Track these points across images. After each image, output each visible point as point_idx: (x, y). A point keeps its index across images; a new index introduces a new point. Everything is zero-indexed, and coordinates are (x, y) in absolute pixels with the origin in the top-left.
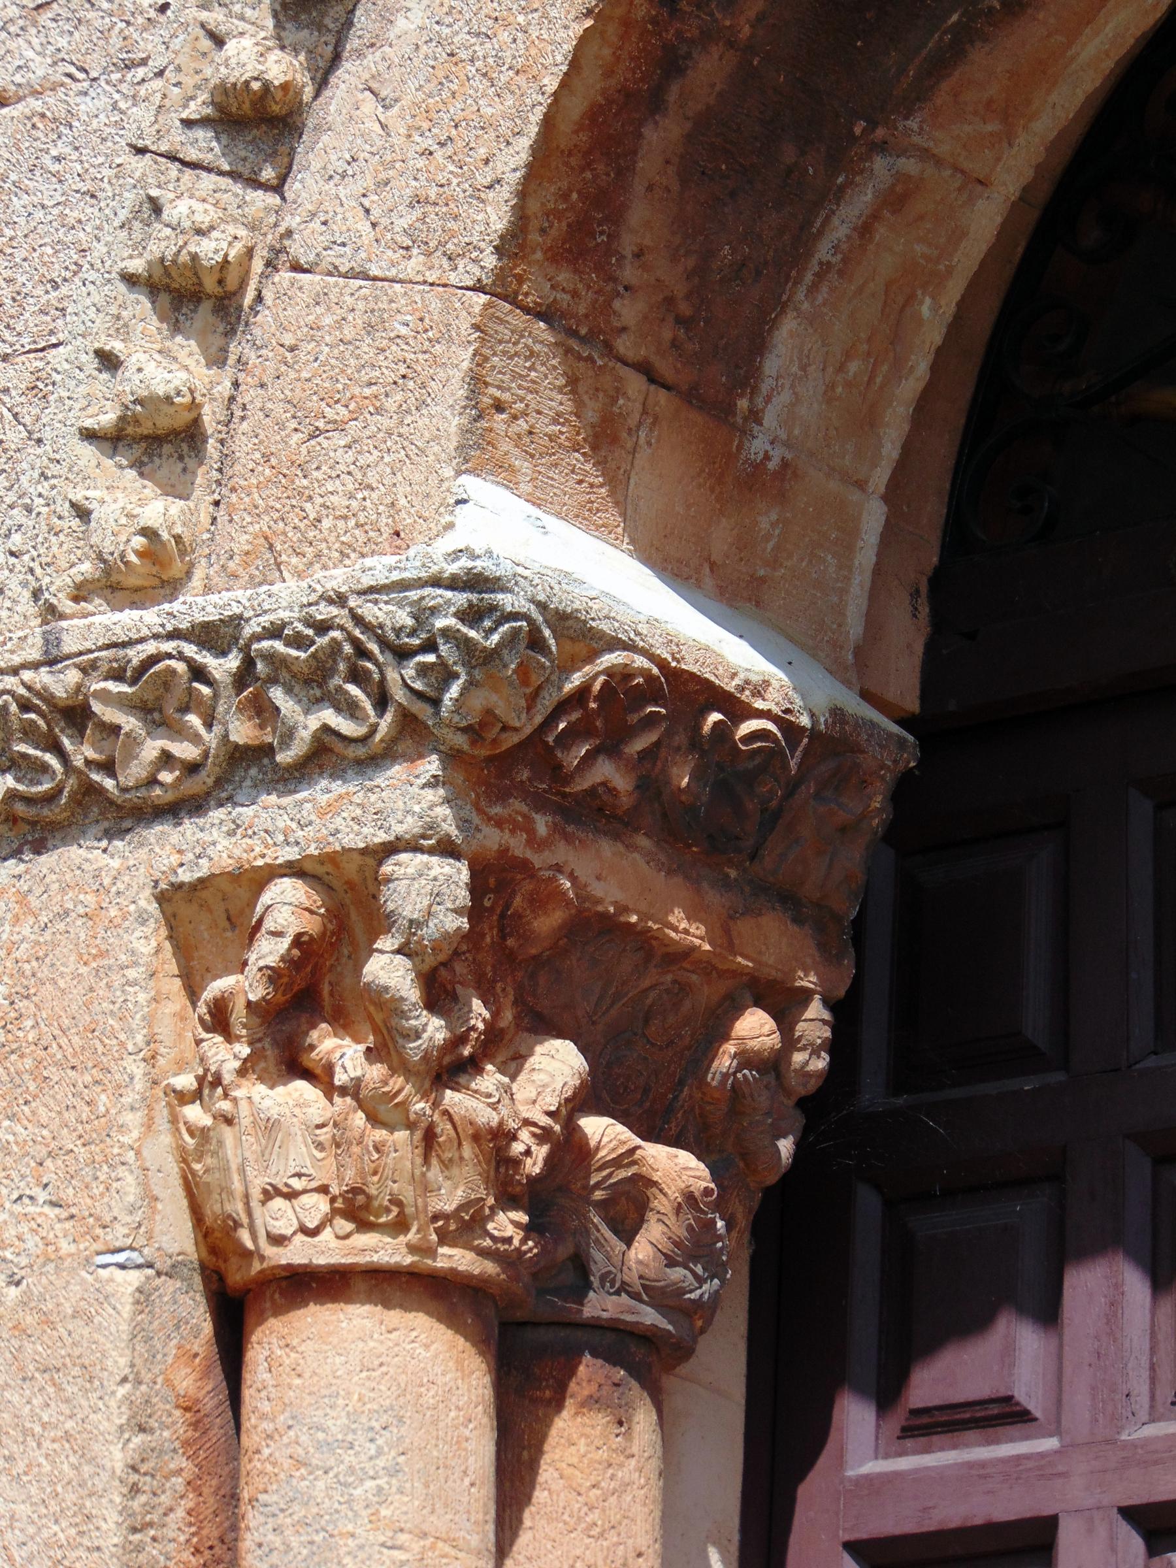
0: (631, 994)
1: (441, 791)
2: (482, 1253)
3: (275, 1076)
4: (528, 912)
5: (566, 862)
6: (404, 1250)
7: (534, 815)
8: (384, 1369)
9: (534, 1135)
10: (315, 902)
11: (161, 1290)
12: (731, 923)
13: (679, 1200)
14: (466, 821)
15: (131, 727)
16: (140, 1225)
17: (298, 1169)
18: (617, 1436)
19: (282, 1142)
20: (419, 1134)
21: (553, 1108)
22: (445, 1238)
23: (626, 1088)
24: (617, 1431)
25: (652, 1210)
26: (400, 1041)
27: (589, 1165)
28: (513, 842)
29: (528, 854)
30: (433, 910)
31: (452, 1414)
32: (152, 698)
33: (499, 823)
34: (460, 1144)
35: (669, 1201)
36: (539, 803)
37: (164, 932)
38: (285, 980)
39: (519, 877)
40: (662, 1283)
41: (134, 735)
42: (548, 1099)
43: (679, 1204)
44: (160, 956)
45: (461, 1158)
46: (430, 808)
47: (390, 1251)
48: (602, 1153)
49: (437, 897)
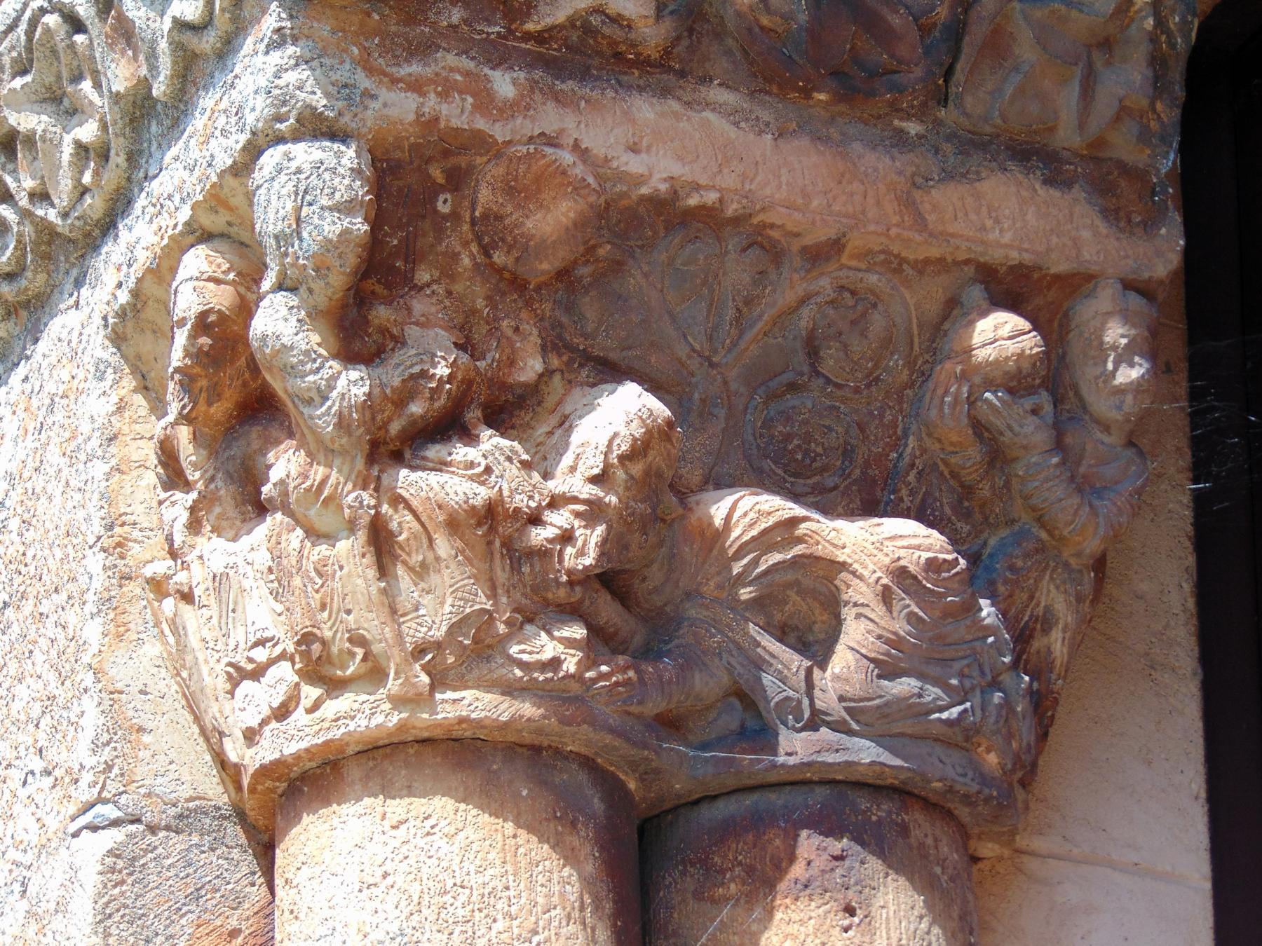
0: (766, 317)
1: (291, 50)
2: (511, 690)
3: (238, 523)
4: (509, 209)
5: (561, 132)
6: (387, 706)
7: (487, 71)
8: (389, 880)
9: (577, 515)
10: (219, 266)
11: (160, 850)
12: (917, 194)
13: (885, 581)
14: (345, 86)
15: (43, 126)
16: (109, 767)
17: (258, 635)
18: (846, 930)
19: (236, 603)
20: (362, 535)
21: (596, 471)
22: (439, 680)
23: (806, 453)
24: (846, 922)
25: (847, 603)
26: (306, 411)
27: (724, 550)
28: (445, 109)
29: (481, 124)
30: (303, 214)
31: (500, 926)
32: (53, 79)
33: (416, 86)
34: (431, 541)
35: (868, 585)
36: (498, 54)
37: (129, 383)
38: (203, 383)
39: (479, 160)
40: (877, 702)
41: (49, 136)
42: (591, 462)
43: (886, 587)
44: (127, 414)
45: (437, 559)
46: (277, 76)
47: (368, 712)
48: (735, 533)
49: (302, 195)
